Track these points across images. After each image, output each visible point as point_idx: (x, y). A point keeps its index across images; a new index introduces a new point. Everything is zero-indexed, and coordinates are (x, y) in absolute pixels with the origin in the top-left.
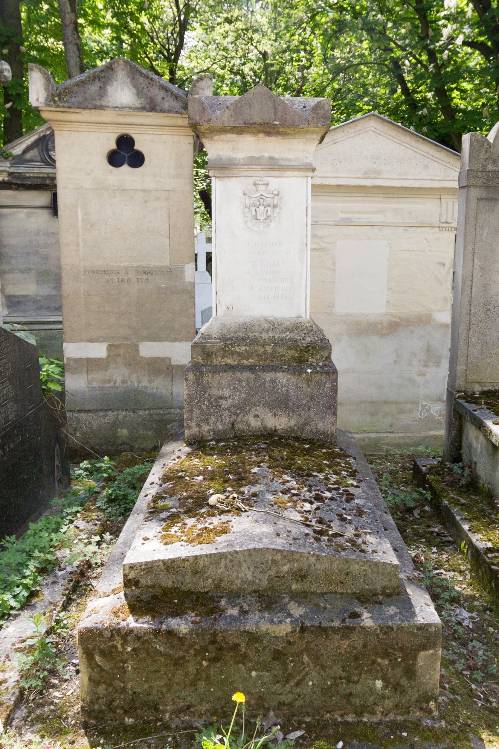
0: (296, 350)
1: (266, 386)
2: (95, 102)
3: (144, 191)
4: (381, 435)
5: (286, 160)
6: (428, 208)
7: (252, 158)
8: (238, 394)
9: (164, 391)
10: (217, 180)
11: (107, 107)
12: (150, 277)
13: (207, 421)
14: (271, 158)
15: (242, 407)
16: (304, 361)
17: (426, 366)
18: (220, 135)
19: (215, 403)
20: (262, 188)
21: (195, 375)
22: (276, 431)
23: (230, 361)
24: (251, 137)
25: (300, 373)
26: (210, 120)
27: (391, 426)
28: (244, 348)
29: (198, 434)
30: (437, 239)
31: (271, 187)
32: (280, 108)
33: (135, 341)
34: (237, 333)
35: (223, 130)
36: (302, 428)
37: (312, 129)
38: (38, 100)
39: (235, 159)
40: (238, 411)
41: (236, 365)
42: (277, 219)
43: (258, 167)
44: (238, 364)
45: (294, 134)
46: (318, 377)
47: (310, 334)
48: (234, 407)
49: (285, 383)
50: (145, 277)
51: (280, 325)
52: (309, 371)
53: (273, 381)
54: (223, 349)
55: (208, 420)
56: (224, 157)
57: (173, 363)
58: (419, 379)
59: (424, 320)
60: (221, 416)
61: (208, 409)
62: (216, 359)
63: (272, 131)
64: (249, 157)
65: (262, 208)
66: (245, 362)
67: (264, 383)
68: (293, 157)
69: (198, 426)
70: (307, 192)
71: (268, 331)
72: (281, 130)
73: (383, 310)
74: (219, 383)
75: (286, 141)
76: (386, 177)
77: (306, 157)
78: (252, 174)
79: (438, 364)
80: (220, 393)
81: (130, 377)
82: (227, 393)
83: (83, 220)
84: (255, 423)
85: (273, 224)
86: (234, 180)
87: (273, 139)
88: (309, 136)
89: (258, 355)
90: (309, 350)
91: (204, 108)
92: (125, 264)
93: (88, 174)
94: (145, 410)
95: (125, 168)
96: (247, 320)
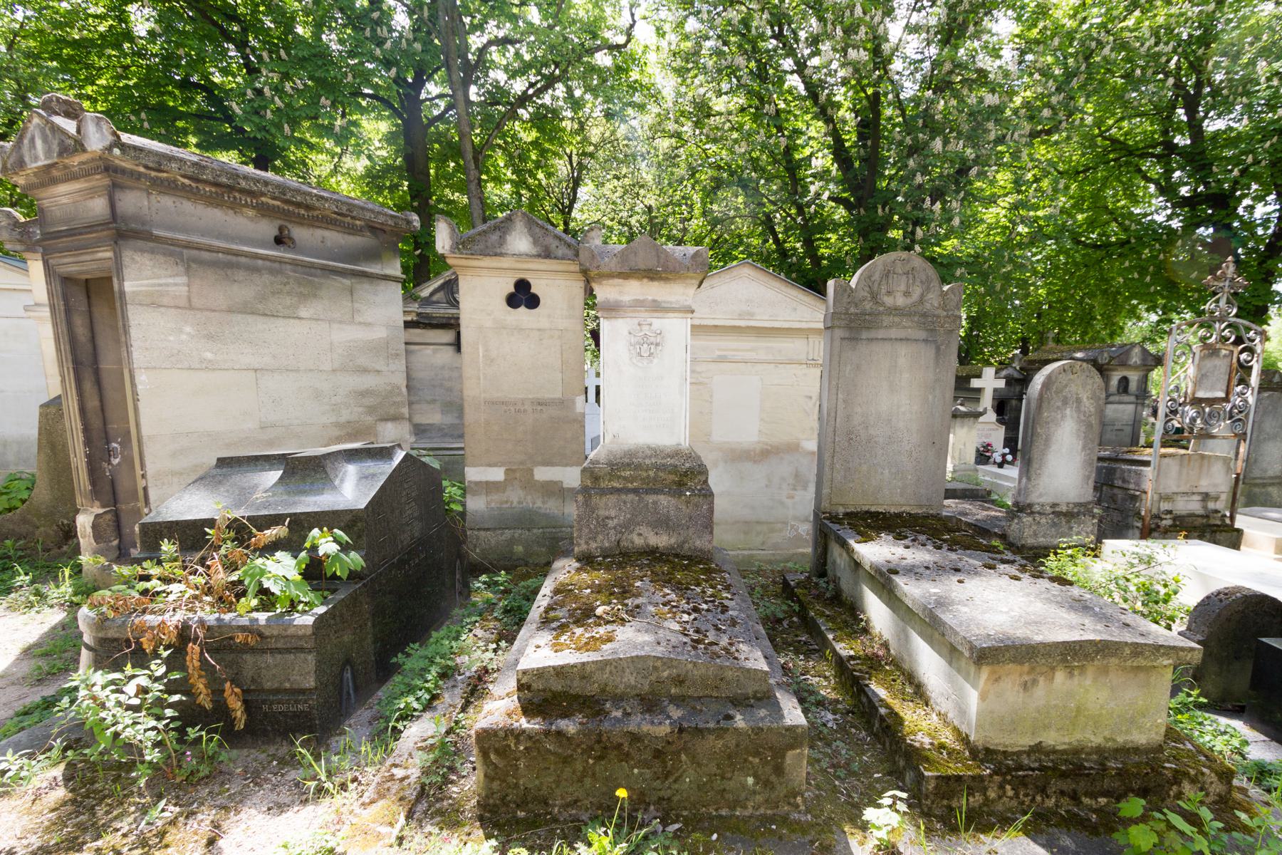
7: (637, 300)
12: (544, 408)
13: (594, 539)
14: (654, 301)
15: (627, 526)
20: (645, 328)
23: (616, 485)
25: (680, 496)
27: (763, 543)
35: (611, 276)
36: (681, 546)
46: (696, 499)
53: (655, 503)
57: (565, 486)
66: (630, 485)
69: (587, 543)
73: (755, 439)
74: (606, 505)
80: (607, 513)
82: (613, 513)
84: (639, 541)
85: (655, 361)
86: (620, 320)
87: (656, 283)
88: (689, 281)
95: (522, 309)
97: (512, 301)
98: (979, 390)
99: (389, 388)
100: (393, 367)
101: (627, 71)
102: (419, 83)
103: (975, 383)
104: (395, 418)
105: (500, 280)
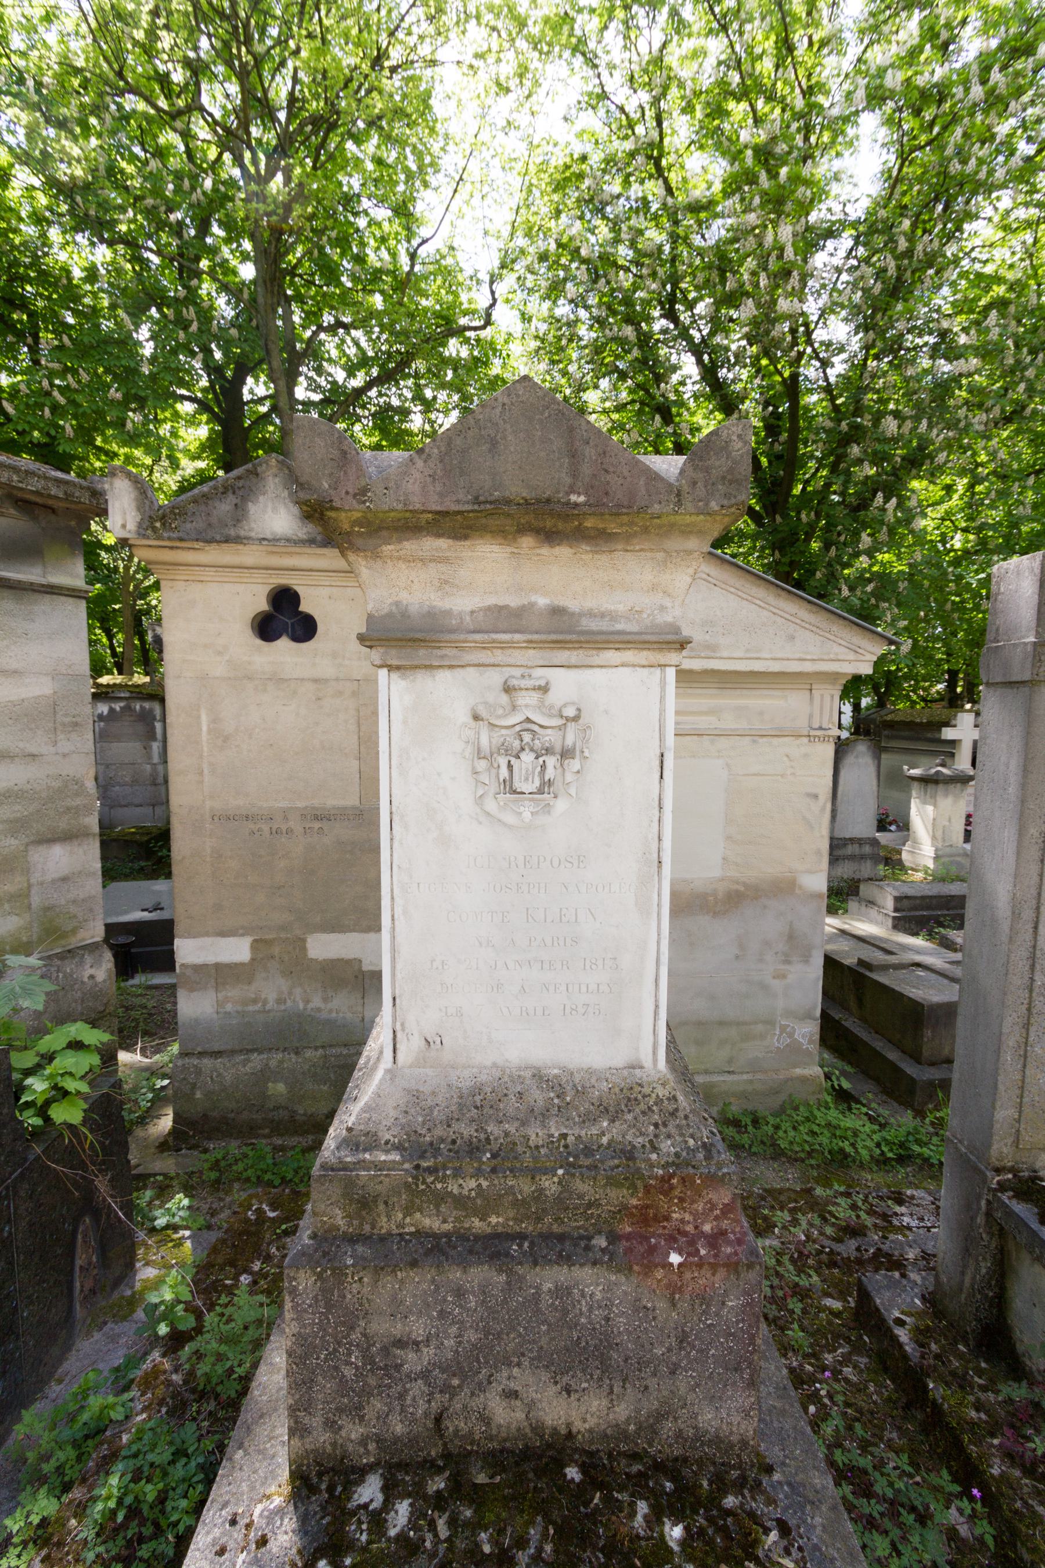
0: (633, 1186)
1: (543, 1306)
2: (226, 531)
3: (316, 681)
4: (716, 1078)
5: (603, 615)
6: (791, 706)
7: (500, 609)
8: (453, 1330)
9: (349, 1015)
10: (395, 676)
11: (248, 538)
12: (325, 825)
13: (357, 1412)
14: (557, 611)
15: (467, 1369)
16: (656, 1219)
17: (787, 962)
18: (400, 541)
19: (384, 1362)
20: (528, 700)
21: (320, 1276)
22: (570, 1435)
23: (431, 1222)
24: (496, 548)
25: (648, 1269)
26: (364, 491)
27: (730, 1061)
28: (473, 1184)
29: (329, 1449)
30: (806, 755)
31: (556, 697)
32: (590, 452)
33: (298, 932)
34: (455, 1126)
35: (411, 525)
36: (650, 1427)
37: (688, 519)
38: (124, 526)
39: (448, 613)
40: (456, 1382)
41: (447, 1235)
42: (573, 791)
43: (517, 637)
44: (456, 1232)
45: (628, 537)
46: (704, 1279)
47: (671, 1128)
48: (443, 1371)
49: (599, 1296)
50: (317, 825)
51: (580, 1092)
52: (675, 1259)
53: (561, 1292)
54: (408, 1186)
55: (359, 1407)
56: (413, 609)
57: (365, 968)
58: (776, 984)
59: (784, 888)
60: (402, 1396)
61: (359, 1375)
62: (389, 1217)
63: (560, 526)
64: (488, 609)
65: (527, 757)
66: (477, 1224)
67: (536, 1298)
68: (621, 608)
69: (330, 1425)
70: (662, 711)
71: (544, 1115)
72: (588, 524)
73: (717, 873)
74: (395, 1301)
75: (604, 558)
76: (725, 654)
77: (662, 608)
78: (499, 656)
79: (806, 959)
80: (398, 1329)
81: (290, 993)
82: (418, 1328)
83: (209, 731)
84: (506, 1416)
85: (561, 805)
86: (444, 677)
87: (563, 551)
88: (675, 543)
89: (515, 1203)
90: (672, 1188)
91: (344, 453)
92: (283, 804)
93: (220, 653)
94: (316, 1048)
95: (284, 643)
96: (483, 1078)
97: (266, 628)
98: (953, 743)
99: (57, 784)
100: (65, 746)
101: (486, 364)
102: (239, 381)
103: (948, 734)
104: (67, 837)
105: (240, 588)
